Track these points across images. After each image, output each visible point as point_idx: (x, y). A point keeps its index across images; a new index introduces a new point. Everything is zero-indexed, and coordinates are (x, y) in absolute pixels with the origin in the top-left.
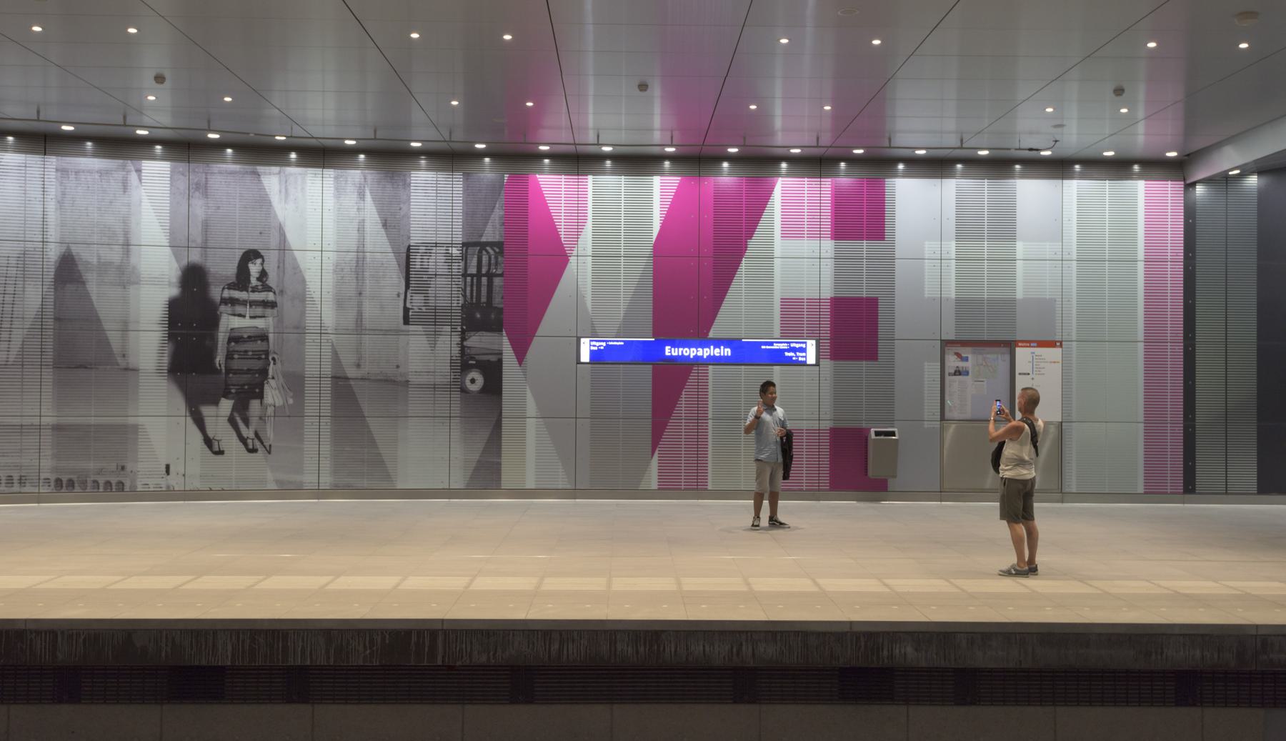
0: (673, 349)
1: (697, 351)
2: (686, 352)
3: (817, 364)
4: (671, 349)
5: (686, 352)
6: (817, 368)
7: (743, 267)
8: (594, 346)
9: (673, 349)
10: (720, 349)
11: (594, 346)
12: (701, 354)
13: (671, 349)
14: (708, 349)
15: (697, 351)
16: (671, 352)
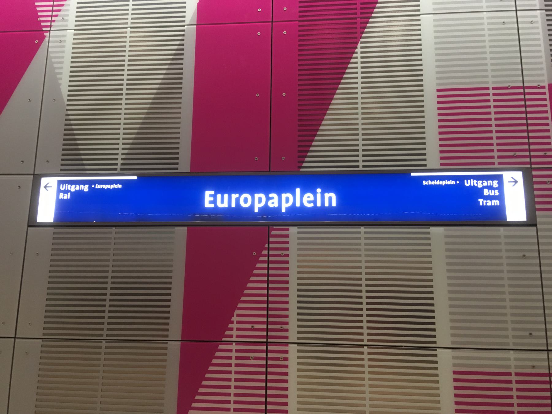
0: (219, 196)
1: (268, 199)
2: (246, 200)
3: (531, 223)
4: (215, 196)
5: (246, 200)
6: (532, 231)
7: (359, 60)
8: (66, 192)
9: (219, 196)
10: (315, 194)
11: (66, 192)
12: (276, 205)
13: (215, 196)
14: (289, 195)
15: (268, 199)
16: (215, 202)
